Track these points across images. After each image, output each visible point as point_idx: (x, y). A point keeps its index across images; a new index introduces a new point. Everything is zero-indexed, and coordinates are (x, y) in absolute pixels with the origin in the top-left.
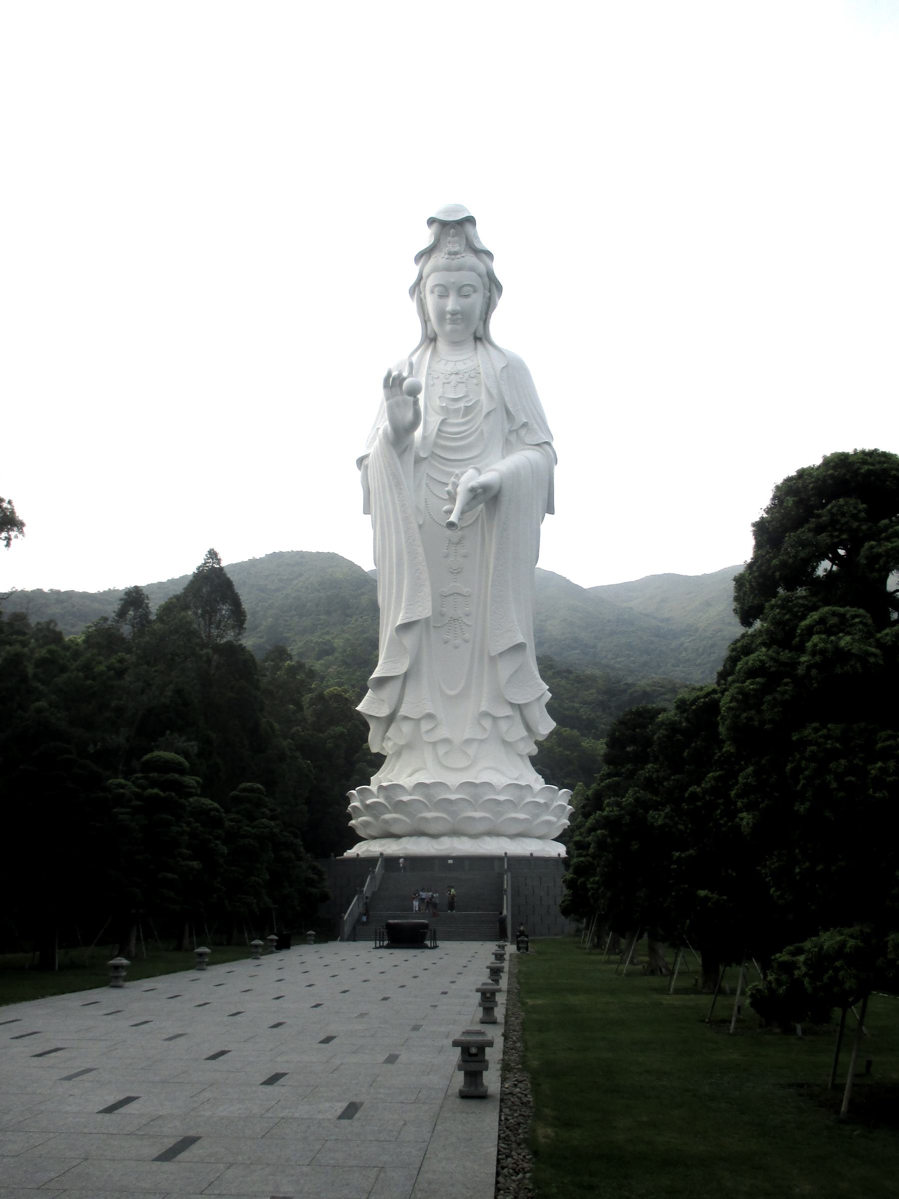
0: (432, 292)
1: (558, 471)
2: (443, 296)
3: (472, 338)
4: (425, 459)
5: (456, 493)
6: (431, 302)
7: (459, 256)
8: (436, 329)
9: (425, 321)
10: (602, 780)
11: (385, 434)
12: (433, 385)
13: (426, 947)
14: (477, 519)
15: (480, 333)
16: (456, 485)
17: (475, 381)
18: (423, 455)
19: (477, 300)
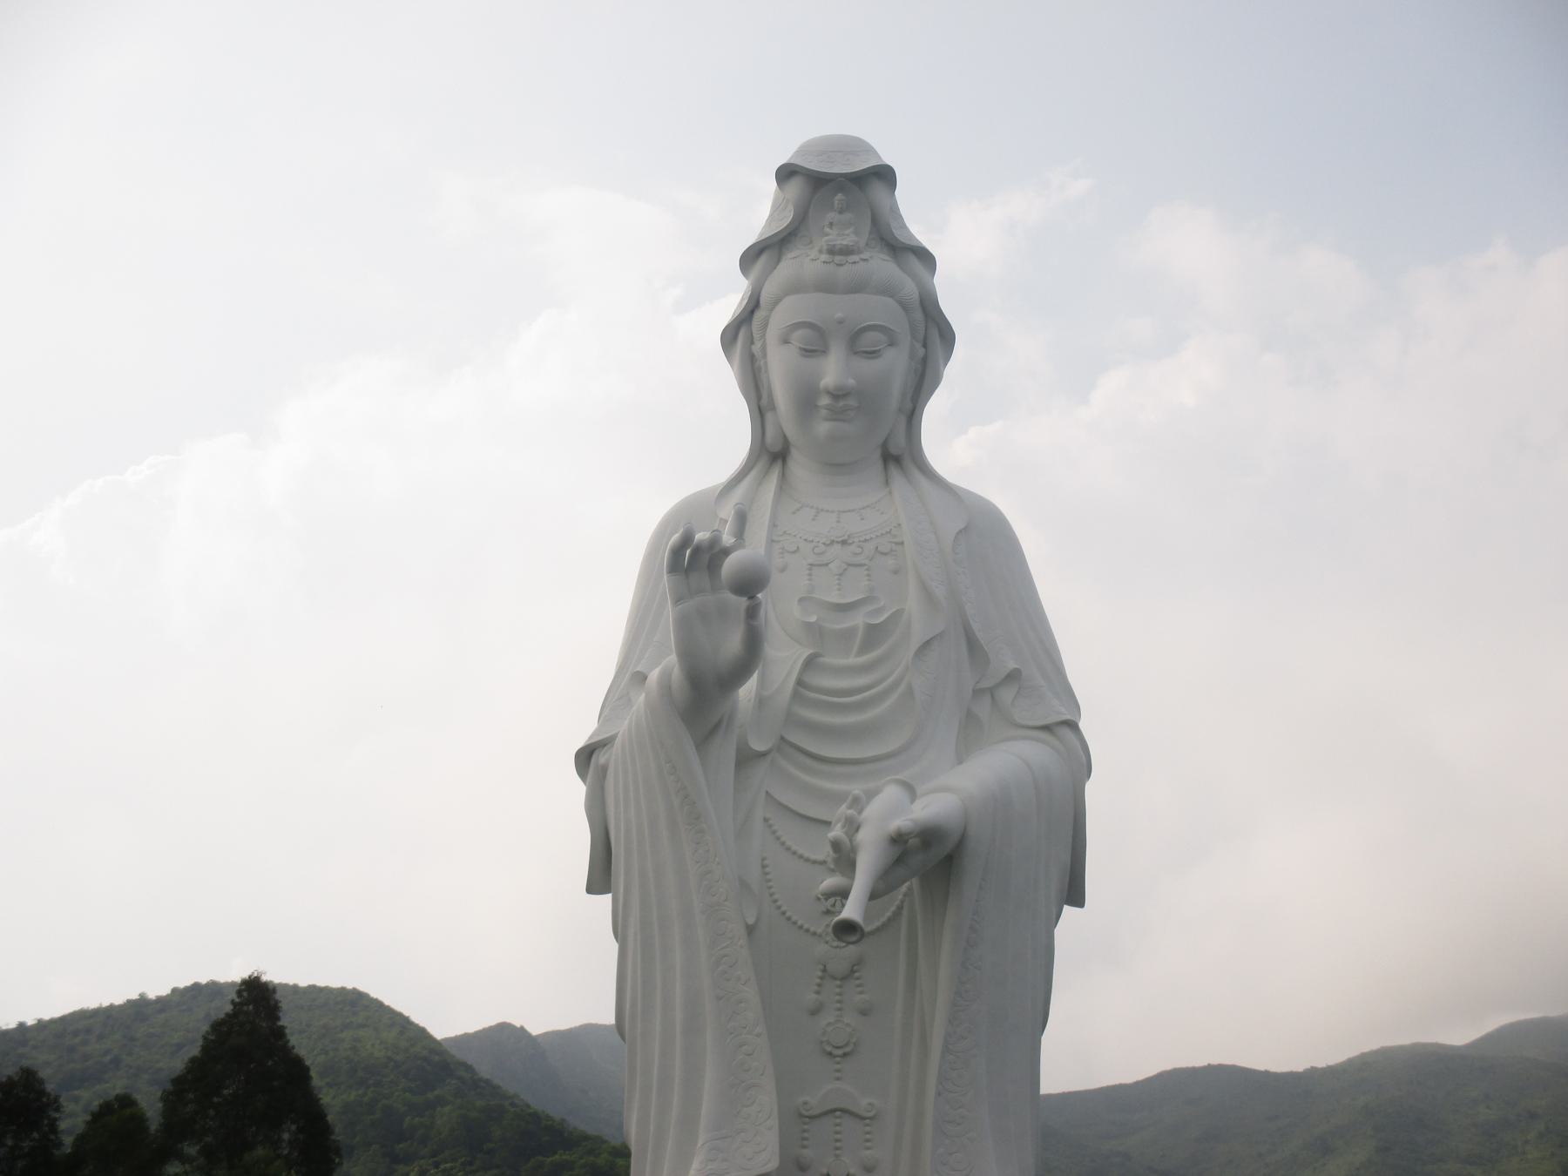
1: (1095, 794)
2: (815, 349)
3: (877, 454)
4: (763, 755)
5: (854, 850)
6: (779, 365)
7: (855, 258)
8: (791, 431)
9: (761, 408)
11: (665, 686)
12: (783, 570)
14: (900, 908)
16: (853, 826)
18: (758, 746)
19: (895, 363)
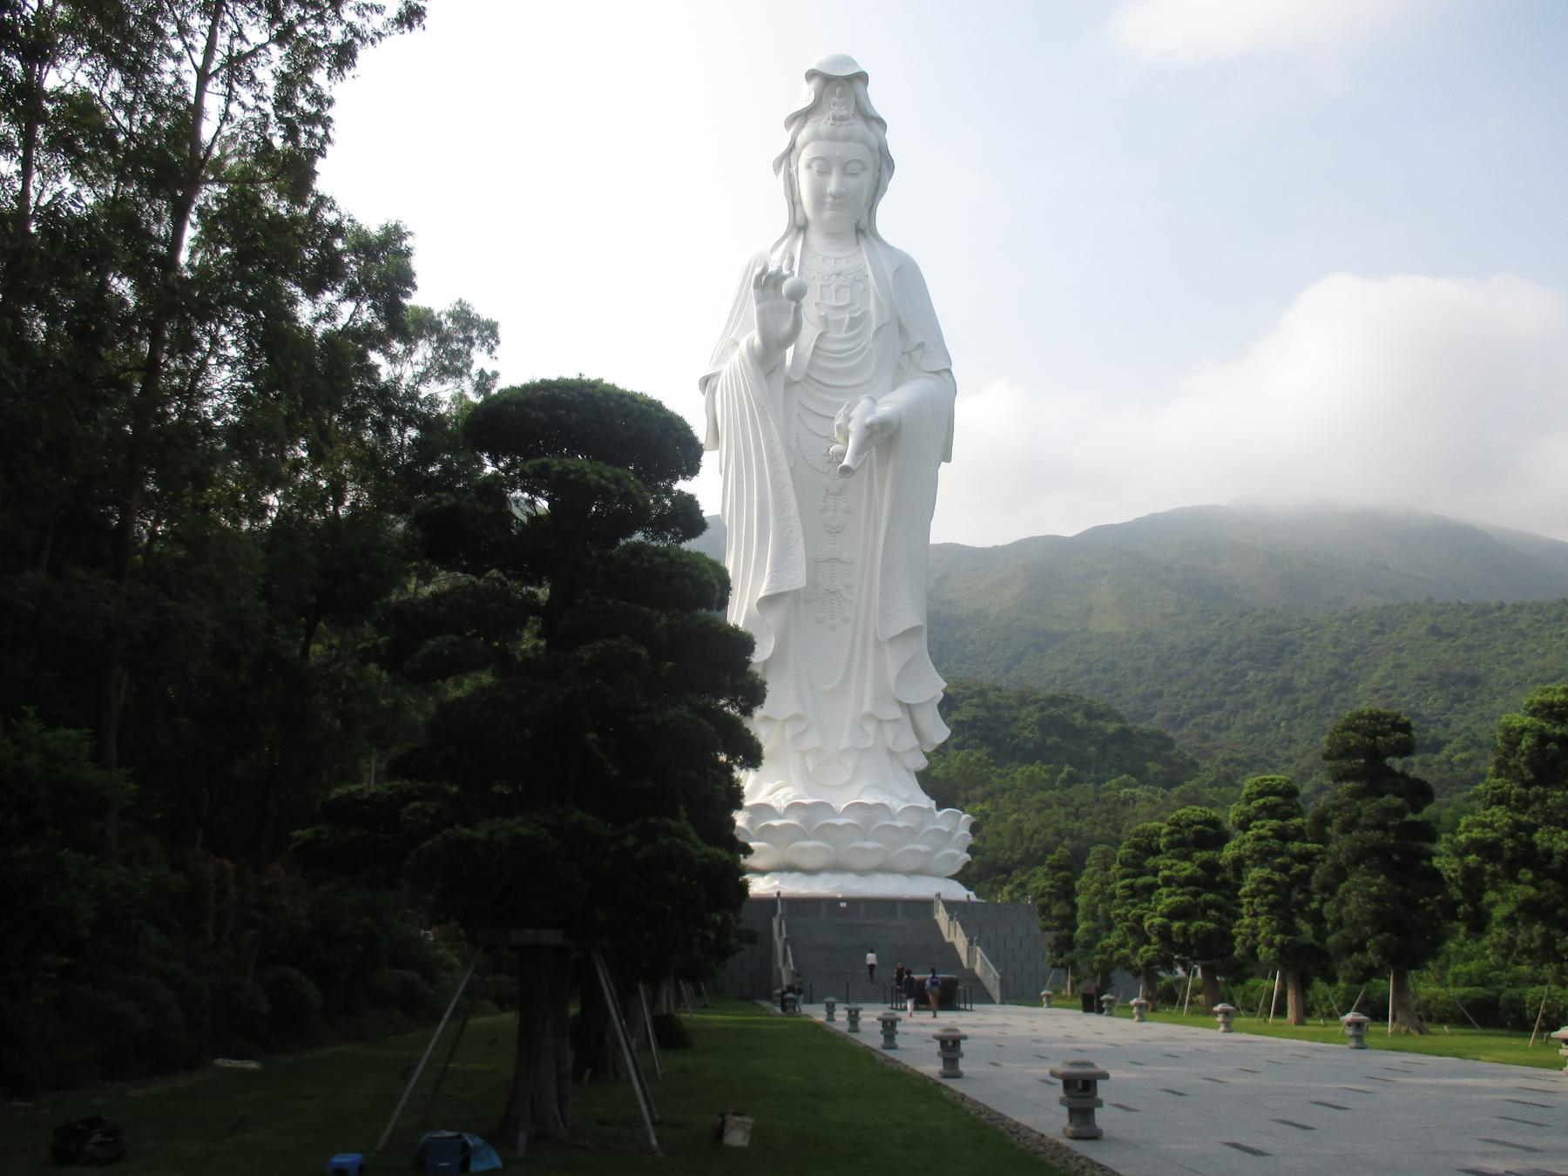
0: (809, 166)
2: (824, 172)
9: (794, 202)
10: (1249, 801)
13: (958, 1009)
15: (864, 224)
17: (862, 286)
18: (795, 378)
19: (866, 179)
